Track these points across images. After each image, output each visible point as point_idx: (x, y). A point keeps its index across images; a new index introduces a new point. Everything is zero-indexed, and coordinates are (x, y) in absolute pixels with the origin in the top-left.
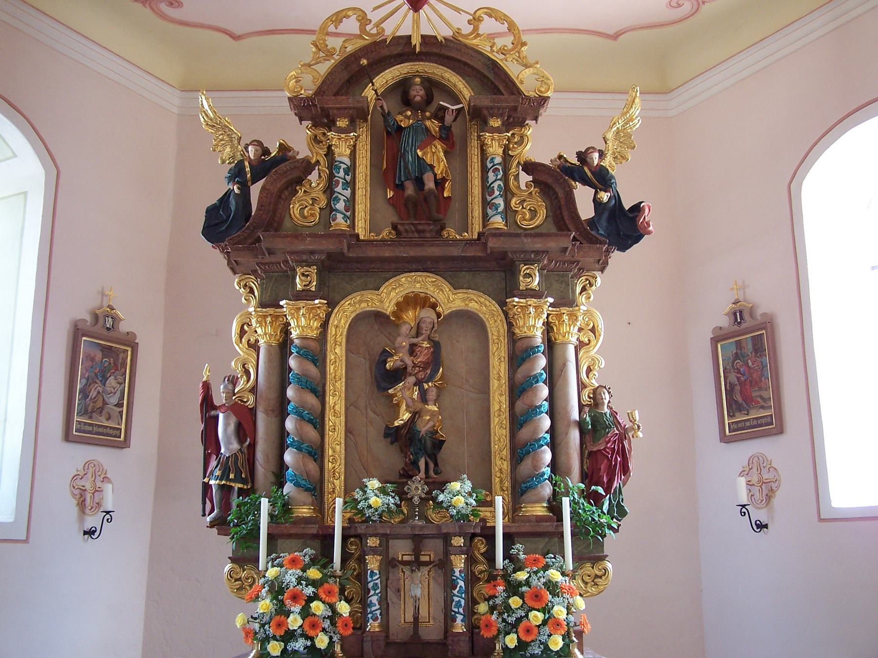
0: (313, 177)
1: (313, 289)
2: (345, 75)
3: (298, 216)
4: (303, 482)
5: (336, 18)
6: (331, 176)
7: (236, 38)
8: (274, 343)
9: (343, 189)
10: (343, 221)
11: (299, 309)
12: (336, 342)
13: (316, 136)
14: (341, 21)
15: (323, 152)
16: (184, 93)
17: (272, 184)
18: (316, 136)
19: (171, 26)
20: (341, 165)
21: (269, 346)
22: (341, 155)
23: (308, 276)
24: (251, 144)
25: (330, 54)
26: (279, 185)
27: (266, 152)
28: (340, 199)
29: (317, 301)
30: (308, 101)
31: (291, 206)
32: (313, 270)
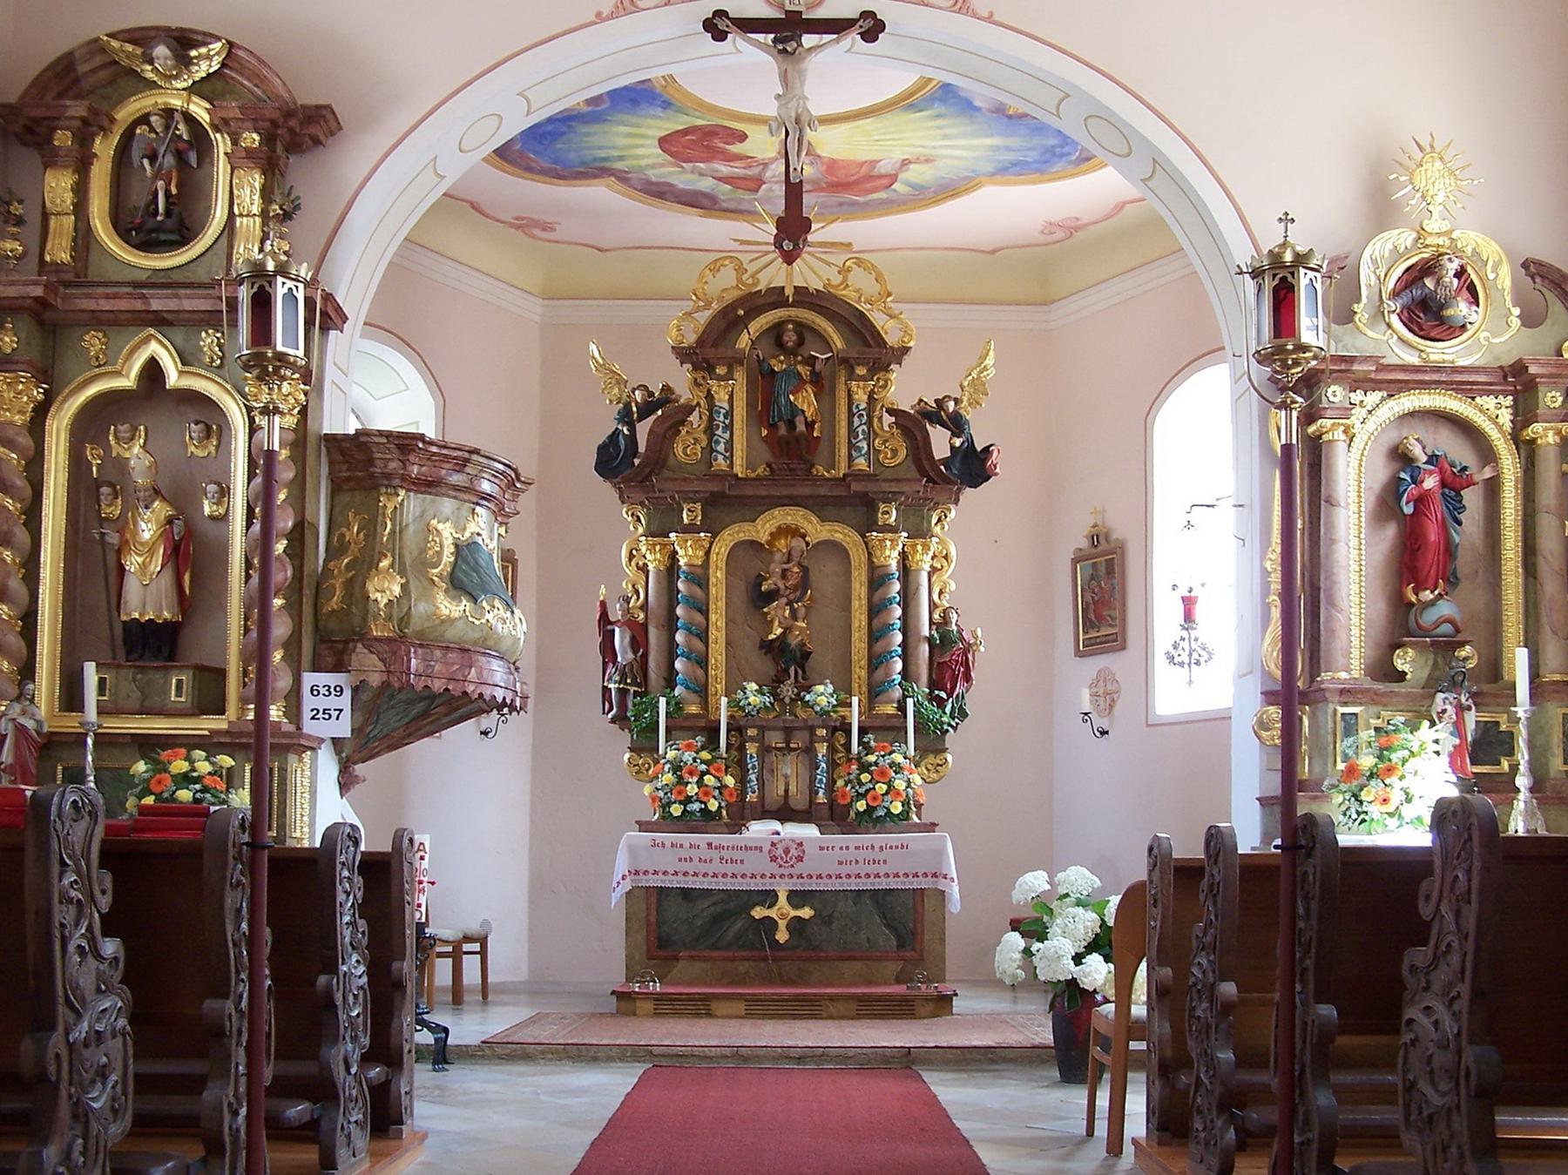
0: (694, 418)
2: (723, 324)
6: (711, 419)
10: (723, 462)
13: (696, 380)
18: (696, 380)
21: (658, 571)
22: (720, 401)
24: (638, 388)
27: (651, 394)
32: (698, 506)
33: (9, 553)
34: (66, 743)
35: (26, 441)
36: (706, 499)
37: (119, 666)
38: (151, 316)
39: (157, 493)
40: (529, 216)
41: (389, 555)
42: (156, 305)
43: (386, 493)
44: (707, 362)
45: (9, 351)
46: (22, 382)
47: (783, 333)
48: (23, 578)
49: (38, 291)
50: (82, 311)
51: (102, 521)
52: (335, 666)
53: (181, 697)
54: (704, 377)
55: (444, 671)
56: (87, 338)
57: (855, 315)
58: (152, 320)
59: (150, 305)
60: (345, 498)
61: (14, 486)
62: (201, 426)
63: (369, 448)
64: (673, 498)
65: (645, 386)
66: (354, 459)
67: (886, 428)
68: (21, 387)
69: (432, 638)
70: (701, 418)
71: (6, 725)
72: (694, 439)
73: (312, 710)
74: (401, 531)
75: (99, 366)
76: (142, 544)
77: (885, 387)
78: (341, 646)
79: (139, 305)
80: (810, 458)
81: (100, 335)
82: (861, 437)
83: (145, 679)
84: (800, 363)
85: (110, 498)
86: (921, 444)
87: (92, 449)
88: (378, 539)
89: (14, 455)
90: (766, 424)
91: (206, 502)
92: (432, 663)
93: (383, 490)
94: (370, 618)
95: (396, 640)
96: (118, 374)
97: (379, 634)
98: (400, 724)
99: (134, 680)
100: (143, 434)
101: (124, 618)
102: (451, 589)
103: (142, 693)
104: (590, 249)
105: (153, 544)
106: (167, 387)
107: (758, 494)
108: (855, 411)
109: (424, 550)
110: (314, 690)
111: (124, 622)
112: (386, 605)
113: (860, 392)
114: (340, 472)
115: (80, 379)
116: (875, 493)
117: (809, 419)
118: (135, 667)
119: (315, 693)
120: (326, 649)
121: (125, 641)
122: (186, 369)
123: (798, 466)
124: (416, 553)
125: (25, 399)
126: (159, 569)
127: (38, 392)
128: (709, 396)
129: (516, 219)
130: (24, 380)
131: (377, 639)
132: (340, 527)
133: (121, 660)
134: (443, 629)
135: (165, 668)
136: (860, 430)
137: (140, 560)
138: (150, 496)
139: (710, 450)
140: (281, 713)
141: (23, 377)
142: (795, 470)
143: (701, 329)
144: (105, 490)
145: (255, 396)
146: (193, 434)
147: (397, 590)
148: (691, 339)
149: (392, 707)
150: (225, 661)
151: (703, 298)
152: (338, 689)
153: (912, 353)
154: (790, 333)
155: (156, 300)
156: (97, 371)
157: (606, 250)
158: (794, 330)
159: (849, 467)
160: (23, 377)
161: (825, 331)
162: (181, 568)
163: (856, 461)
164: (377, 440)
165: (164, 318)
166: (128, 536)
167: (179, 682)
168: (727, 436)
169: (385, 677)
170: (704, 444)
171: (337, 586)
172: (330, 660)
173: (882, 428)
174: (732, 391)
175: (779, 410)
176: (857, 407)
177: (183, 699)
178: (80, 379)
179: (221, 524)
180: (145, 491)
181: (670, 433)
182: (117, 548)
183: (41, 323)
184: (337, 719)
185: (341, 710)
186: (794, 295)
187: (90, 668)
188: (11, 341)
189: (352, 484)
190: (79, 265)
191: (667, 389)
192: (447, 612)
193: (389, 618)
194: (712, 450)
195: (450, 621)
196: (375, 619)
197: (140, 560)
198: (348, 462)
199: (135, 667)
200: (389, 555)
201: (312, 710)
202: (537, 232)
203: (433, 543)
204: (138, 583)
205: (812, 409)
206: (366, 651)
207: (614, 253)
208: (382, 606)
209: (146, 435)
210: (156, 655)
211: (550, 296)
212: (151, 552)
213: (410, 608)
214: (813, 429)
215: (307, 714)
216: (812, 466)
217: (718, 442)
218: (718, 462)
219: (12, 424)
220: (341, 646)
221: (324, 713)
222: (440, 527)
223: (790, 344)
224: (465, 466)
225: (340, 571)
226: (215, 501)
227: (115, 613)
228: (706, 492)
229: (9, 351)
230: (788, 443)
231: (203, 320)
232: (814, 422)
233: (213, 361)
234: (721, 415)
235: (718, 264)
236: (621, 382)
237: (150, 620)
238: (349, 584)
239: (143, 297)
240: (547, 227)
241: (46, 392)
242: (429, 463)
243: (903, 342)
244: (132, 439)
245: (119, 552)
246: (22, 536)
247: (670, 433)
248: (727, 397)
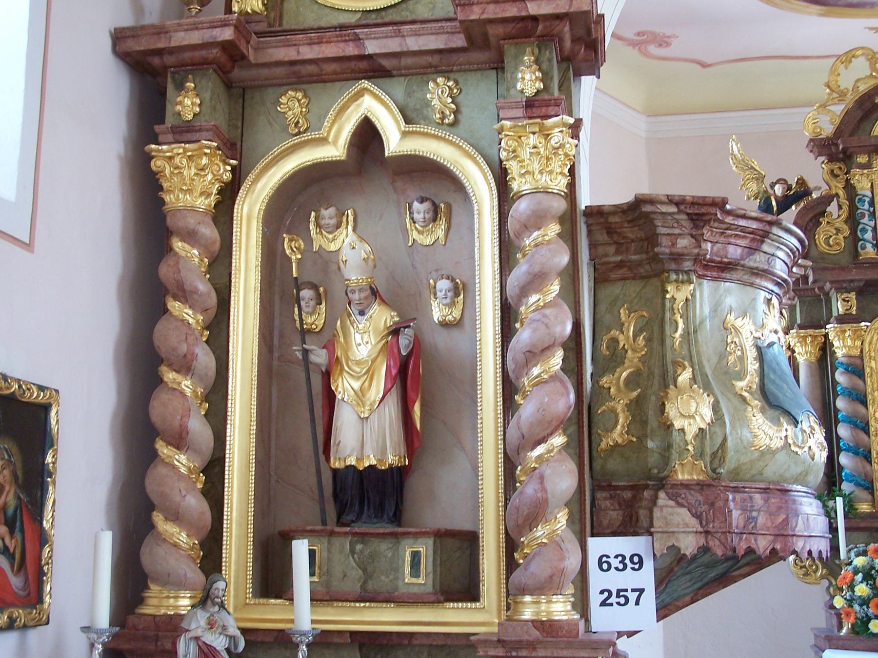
0: (833, 208)
1: (854, 313)
2: (860, 114)
3: (824, 245)
4: (863, 482)
5: (846, 59)
6: (853, 208)
7: (704, 65)
8: (813, 359)
9: (870, 220)
10: (872, 250)
11: (845, 331)
12: (870, 357)
13: (832, 171)
14: (850, 62)
15: (841, 186)
16: (653, 119)
17: (801, 218)
18: (832, 171)
19: (656, 62)
20: (865, 198)
21: (810, 364)
22: (862, 189)
23: (848, 301)
24: (777, 182)
25: (842, 94)
26: (807, 219)
27: (790, 188)
28: (867, 230)
29: (863, 324)
30: (829, 141)
31: (817, 237)
32: (853, 295)
33: (188, 383)
34: (263, 642)
35: (209, 232)
37: (332, 534)
38: (363, 65)
39: (375, 293)
40: (649, 29)
41: (686, 363)
42: (372, 47)
43: (677, 281)
45: (190, 117)
46: (206, 154)
48: (206, 415)
49: (227, 34)
50: (279, 64)
51: (305, 333)
52: (623, 523)
53: (418, 576)
55: (769, 524)
56: (284, 100)
58: (366, 71)
59: (365, 48)
60: (614, 290)
61: (195, 291)
62: (427, 205)
63: (652, 221)
65: (785, 180)
66: (624, 238)
68: (204, 161)
69: (748, 476)
71: (187, 647)
72: (836, 229)
73: (602, 592)
74: (695, 332)
75: (299, 133)
76: (358, 363)
78: (628, 495)
79: (351, 50)
81: (300, 95)
83: (367, 552)
85: (312, 303)
87: (291, 240)
88: (668, 342)
89: (195, 252)
91: (434, 304)
92: (754, 514)
93: (673, 277)
94: (674, 455)
95: (709, 486)
96: (323, 141)
97: (686, 477)
98: (687, 591)
99: (352, 552)
100: (351, 218)
101: (336, 464)
102: (766, 407)
103: (365, 571)
104: (687, 64)
105: (374, 361)
106: (386, 155)
109: (723, 356)
110: (603, 563)
111: (335, 471)
112: (696, 437)
114: (606, 255)
115: (276, 151)
118: (355, 534)
119: (605, 566)
120: (605, 499)
121: (336, 495)
122: (412, 128)
124: (714, 360)
125: (210, 177)
126: (381, 395)
127: (225, 171)
128: (850, 188)
129: (638, 34)
130: (208, 151)
131: (686, 485)
132: (609, 330)
133: (331, 525)
134: (761, 464)
135: (394, 535)
137: (356, 385)
138: (366, 298)
139: (854, 239)
140: (569, 607)
141: (209, 148)
143: (838, 121)
144: (306, 294)
145: (514, 151)
146: (416, 216)
147: (707, 413)
148: (828, 129)
149: (687, 574)
150: (476, 519)
151: (837, 90)
152: (636, 559)
155: (372, 41)
156: (297, 140)
157: (709, 65)
160: (209, 148)
162: (410, 393)
164: (664, 209)
165: (381, 66)
166: (339, 353)
167: (415, 556)
169: (702, 541)
170: (847, 233)
171: (619, 410)
172: (614, 515)
177: (421, 581)
178: (276, 151)
179: (455, 333)
180: (360, 290)
182: (324, 369)
183: (228, 85)
184: (637, 603)
185: (641, 591)
187: (300, 549)
188: (193, 104)
189: (623, 271)
190: (272, 15)
191: (801, 182)
192: (767, 442)
193: (700, 454)
195: (770, 452)
196: (680, 454)
197: (356, 385)
198: (615, 243)
199: (355, 534)
200: (686, 363)
201: (602, 592)
202: (653, 49)
203: (733, 346)
204: (355, 417)
206: (672, 503)
207: (716, 67)
208: (689, 437)
209: (355, 220)
210: (379, 513)
211: (652, 113)
212: (370, 374)
213: (725, 439)
215: (595, 599)
217: (864, 231)
219: (193, 210)
220: (628, 495)
221: (618, 596)
222: (739, 323)
224: (762, 242)
225: (618, 389)
226: (445, 301)
227: (322, 458)
229: (190, 117)
231: (430, 66)
233: (443, 119)
234: (866, 203)
235: (850, 56)
236: (760, 179)
237: (370, 466)
238: (636, 407)
239: (357, 39)
240: (663, 41)
241: (234, 170)
242: (722, 239)
244: (338, 226)
245: (327, 376)
246: (205, 359)
247: (811, 224)
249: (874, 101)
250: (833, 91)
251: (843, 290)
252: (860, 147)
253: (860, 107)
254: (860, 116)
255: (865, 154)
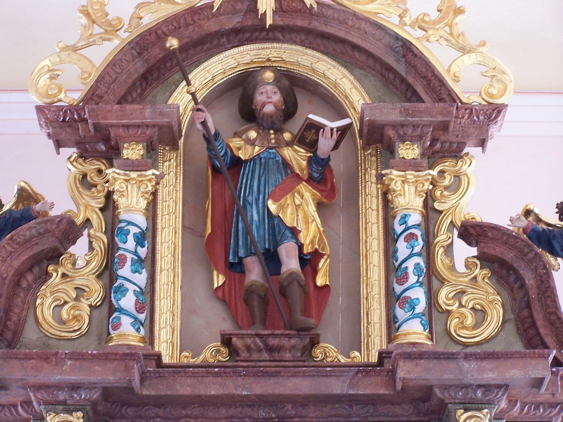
9: (134, 272)
10: (131, 330)
13: (85, 176)
18: (85, 176)
22: (129, 210)
30: (72, 113)
31: (38, 301)
36: (94, 404)
44: (107, 140)
47: (255, 88)
54: (100, 171)
57: (393, 49)
64: (27, 403)
67: (461, 267)
70: (91, 248)
77: (455, 187)
80: (312, 321)
82: (413, 279)
84: (289, 144)
86: (533, 294)
90: (222, 264)
107: (202, 392)
108: (399, 229)
113: (410, 190)
116: (445, 387)
117: (307, 249)
123: (285, 342)
136: (410, 265)
142: (279, 349)
153: (508, 115)
154: (269, 88)
158: (277, 81)
159: (390, 339)
161: (336, 85)
163: (404, 328)
168: (142, 278)
173: (452, 268)
174: (155, 194)
175: (248, 232)
176: (404, 219)
181: (30, 277)
186: (274, 12)
194: (112, 310)
205: (313, 227)
214: (315, 272)
216: (314, 342)
217: (122, 291)
218: (122, 330)
223: (269, 109)
228: (91, 387)
230: (265, 301)
232: (317, 255)
234: (131, 238)
243: (491, 96)
248: (143, 204)
249: (165, 45)
250: (94, 22)
251: (61, 407)
252: (127, 126)
253: (140, 54)
254: (142, 71)
255: (138, 142)
